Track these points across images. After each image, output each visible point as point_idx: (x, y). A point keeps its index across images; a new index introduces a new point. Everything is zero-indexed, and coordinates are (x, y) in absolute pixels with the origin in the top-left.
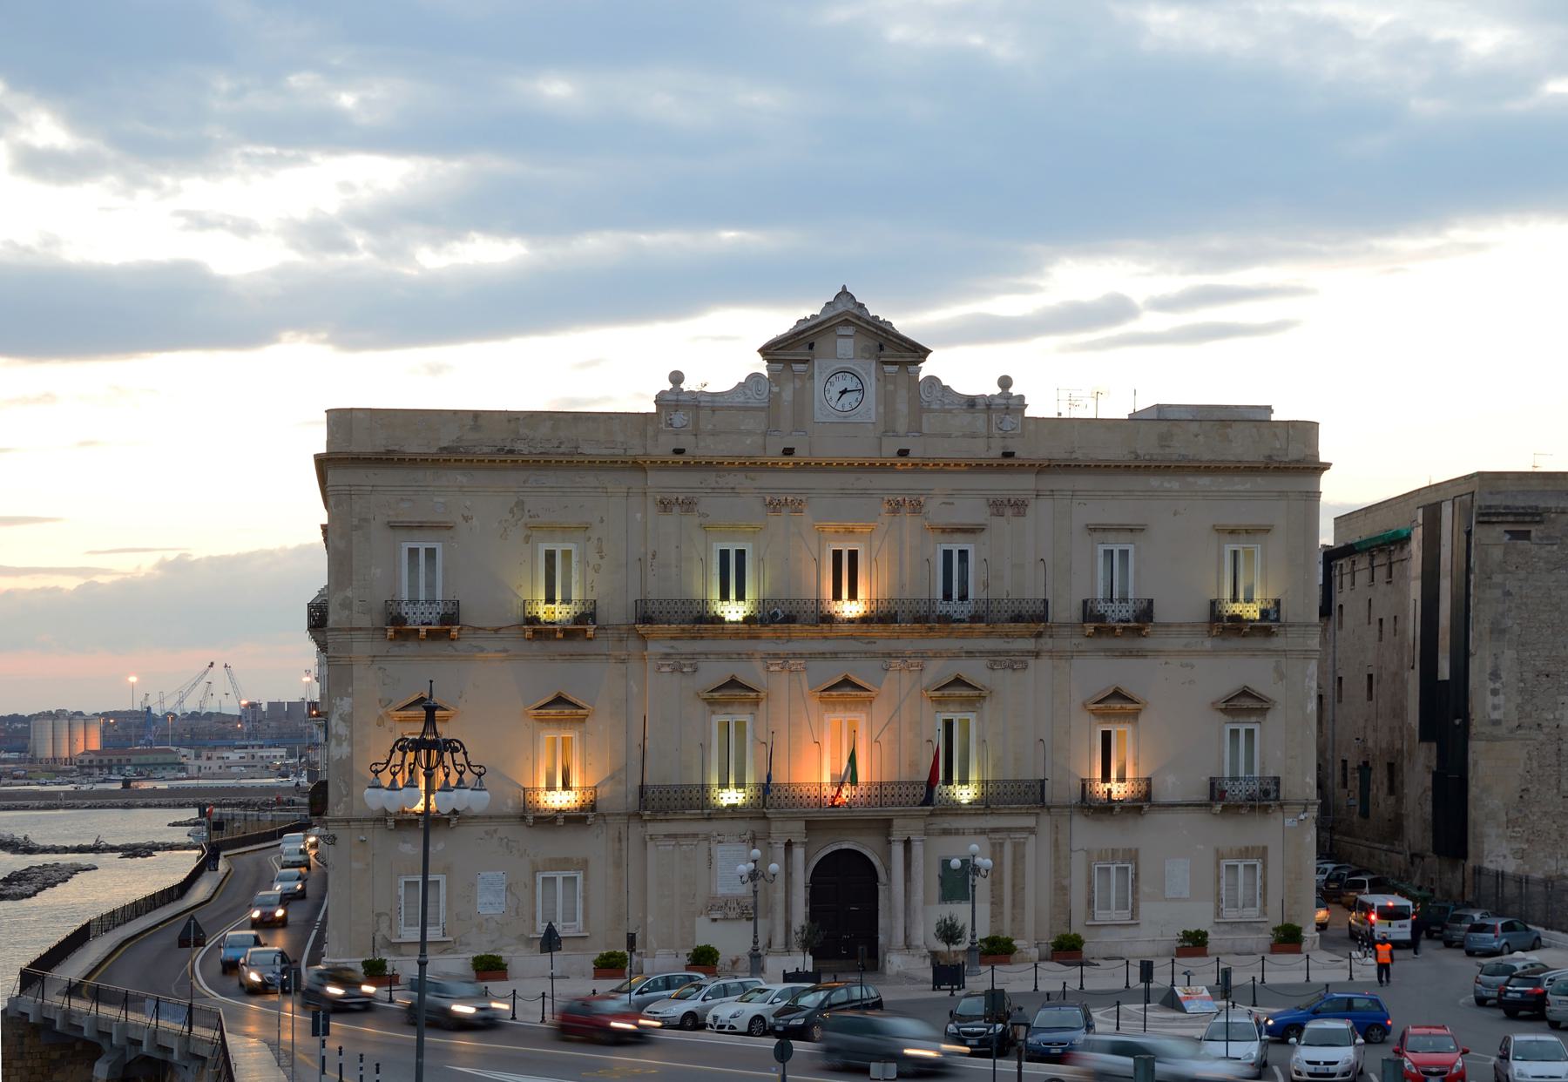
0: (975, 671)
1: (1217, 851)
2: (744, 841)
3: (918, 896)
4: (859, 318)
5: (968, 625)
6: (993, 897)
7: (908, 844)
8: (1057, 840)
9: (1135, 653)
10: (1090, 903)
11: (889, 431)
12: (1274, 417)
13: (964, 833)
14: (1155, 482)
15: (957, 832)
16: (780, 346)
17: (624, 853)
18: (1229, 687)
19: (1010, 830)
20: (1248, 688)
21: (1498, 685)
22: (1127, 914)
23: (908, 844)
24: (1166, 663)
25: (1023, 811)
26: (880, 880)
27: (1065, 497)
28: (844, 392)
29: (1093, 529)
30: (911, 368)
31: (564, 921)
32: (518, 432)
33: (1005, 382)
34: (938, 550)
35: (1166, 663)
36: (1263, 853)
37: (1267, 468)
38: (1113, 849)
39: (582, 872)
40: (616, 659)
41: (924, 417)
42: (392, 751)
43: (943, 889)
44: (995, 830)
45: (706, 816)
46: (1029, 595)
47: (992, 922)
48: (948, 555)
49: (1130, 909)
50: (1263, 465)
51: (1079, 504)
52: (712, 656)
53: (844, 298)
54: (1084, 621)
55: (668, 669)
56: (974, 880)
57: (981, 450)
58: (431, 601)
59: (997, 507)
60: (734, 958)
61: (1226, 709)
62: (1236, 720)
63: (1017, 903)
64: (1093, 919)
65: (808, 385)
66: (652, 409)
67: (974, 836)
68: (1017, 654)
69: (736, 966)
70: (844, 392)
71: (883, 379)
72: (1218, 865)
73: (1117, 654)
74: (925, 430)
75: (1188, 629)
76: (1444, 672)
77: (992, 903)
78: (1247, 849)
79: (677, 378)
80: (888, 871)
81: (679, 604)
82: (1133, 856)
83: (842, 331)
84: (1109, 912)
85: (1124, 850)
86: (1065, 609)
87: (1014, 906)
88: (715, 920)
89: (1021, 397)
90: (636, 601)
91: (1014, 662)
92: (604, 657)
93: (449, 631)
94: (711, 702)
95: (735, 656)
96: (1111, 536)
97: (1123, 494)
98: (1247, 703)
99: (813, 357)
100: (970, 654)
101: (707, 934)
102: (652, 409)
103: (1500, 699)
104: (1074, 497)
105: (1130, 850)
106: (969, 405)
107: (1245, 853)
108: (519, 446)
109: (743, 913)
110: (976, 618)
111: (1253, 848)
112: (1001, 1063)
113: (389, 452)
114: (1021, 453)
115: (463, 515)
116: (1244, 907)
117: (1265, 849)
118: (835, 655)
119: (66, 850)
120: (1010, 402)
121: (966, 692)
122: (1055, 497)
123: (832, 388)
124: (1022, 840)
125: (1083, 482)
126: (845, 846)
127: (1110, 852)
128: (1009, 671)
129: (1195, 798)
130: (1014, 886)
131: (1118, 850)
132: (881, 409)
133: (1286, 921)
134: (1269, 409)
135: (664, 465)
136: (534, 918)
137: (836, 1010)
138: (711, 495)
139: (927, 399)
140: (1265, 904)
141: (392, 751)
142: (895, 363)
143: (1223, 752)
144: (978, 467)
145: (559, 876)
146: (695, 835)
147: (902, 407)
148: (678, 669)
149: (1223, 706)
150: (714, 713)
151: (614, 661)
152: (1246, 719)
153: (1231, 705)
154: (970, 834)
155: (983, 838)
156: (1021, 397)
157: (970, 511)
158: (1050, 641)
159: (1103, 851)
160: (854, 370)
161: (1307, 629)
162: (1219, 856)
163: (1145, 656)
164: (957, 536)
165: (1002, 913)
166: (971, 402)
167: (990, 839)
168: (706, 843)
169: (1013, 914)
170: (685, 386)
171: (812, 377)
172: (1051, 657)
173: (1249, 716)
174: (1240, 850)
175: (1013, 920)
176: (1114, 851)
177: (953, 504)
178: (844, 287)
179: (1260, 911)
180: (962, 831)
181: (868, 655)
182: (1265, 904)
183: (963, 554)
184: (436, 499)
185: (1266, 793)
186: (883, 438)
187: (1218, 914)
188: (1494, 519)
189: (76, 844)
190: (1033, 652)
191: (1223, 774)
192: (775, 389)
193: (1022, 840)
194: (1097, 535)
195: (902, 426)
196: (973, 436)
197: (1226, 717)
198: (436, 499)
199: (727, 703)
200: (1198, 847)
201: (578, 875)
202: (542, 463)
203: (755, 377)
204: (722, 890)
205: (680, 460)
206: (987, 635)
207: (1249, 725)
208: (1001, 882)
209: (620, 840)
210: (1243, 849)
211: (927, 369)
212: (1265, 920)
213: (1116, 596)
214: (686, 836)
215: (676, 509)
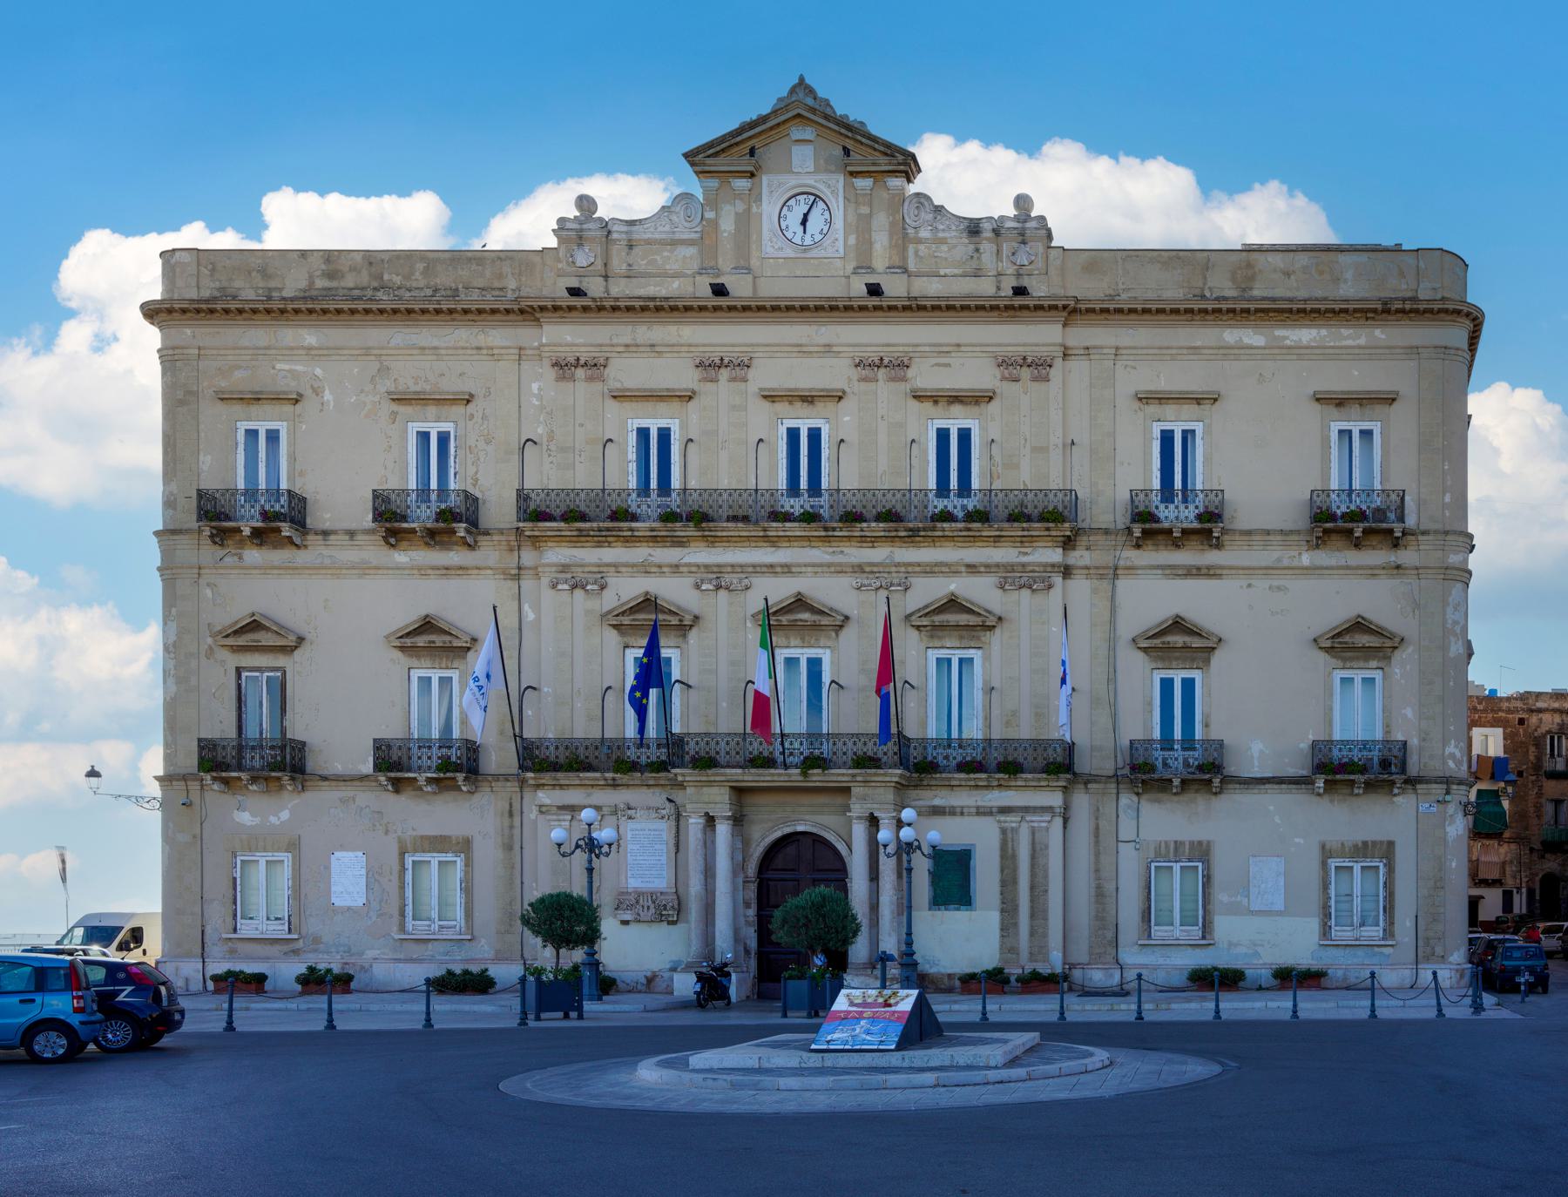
0: (980, 591)
1: (1323, 847)
2: (663, 818)
4: (813, 110)
5: (961, 525)
6: (1003, 903)
8: (1097, 828)
9: (1204, 571)
11: (864, 267)
13: (962, 814)
14: (1232, 335)
15: (952, 812)
16: (711, 151)
17: (517, 832)
18: (1338, 614)
19: (1026, 810)
20: (1363, 618)
22: (1196, 931)
24: (1249, 585)
25: (1043, 784)
27: (1105, 357)
28: (804, 222)
29: (1145, 399)
32: (382, 278)
34: (930, 428)
35: (1249, 585)
36: (1387, 851)
38: (1176, 842)
39: (462, 855)
40: (504, 574)
41: (911, 249)
43: (935, 890)
44: (1005, 810)
45: (610, 782)
47: (1003, 936)
48: (943, 435)
49: (1200, 925)
50: (1379, 307)
51: (1126, 366)
52: (623, 569)
55: (566, 587)
56: (909, 862)
60: (649, 974)
61: (1332, 648)
62: (1348, 665)
63: (1038, 912)
64: (1149, 936)
65: (754, 209)
66: (552, 242)
67: (976, 818)
68: (1037, 569)
69: (652, 984)
70: (804, 222)
71: (852, 198)
72: (1324, 864)
73: (1180, 573)
74: (912, 267)
75: (1279, 538)
77: (1002, 911)
78: (1365, 843)
81: (572, 495)
82: (1202, 852)
83: (797, 132)
84: (1172, 928)
85: (1191, 843)
87: (1033, 916)
88: (625, 923)
92: (489, 572)
95: (653, 569)
96: (1170, 410)
97: (1185, 351)
98: (1363, 640)
99: (758, 168)
100: (972, 569)
104: (1119, 357)
105: (1200, 843)
106: (970, 232)
107: (1363, 850)
109: (662, 915)
110: (972, 516)
111: (1374, 843)
112: (982, 475)
114: (1039, 289)
115: (312, 386)
116: (1363, 924)
117: (1391, 844)
118: (787, 569)
121: (963, 619)
122: (1092, 357)
123: (788, 214)
124: (1044, 824)
126: (800, 828)
127: (1172, 846)
128: (1026, 593)
129: (1291, 771)
130: (1032, 888)
131: (1182, 843)
132: (852, 240)
138: (624, 355)
139: (914, 224)
143: (1331, 709)
145: (435, 859)
149: (1328, 644)
151: (502, 577)
152: (1362, 664)
153: (1340, 643)
154: (969, 814)
157: (974, 374)
158: (1086, 554)
159: (1163, 845)
160: (814, 187)
161: (1448, 538)
162: (1326, 853)
163: (1219, 576)
164: (957, 409)
165: (1016, 925)
167: (999, 822)
168: (615, 817)
169: (1032, 927)
172: (1088, 577)
173: (1366, 659)
174: (1356, 846)
175: (1032, 934)
176: (1178, 845)
177: (949, 365)
178: (802, 79)
179: (1385, 930)
180: (958, 810)
181: (832, 569)
182: (1390, 922)
183: (965, 435)
184: (278, 366)
185: (1385, 764)
186: (853, 277)
187: (1324, 935)
190: (1059, 567)
191: (1331, 735)
192: (710, 215)
193: (1044, 824)
194: (1153, 409)
197: (1334, 660)
198: (278, 366)
200: (1297, 840)
201: (458, 859)
204: (633, 883)
207: (1367, 671)
208: (1015, 881)
209: (511, 814)
210: (1360, 844)
212: (1390, 943)
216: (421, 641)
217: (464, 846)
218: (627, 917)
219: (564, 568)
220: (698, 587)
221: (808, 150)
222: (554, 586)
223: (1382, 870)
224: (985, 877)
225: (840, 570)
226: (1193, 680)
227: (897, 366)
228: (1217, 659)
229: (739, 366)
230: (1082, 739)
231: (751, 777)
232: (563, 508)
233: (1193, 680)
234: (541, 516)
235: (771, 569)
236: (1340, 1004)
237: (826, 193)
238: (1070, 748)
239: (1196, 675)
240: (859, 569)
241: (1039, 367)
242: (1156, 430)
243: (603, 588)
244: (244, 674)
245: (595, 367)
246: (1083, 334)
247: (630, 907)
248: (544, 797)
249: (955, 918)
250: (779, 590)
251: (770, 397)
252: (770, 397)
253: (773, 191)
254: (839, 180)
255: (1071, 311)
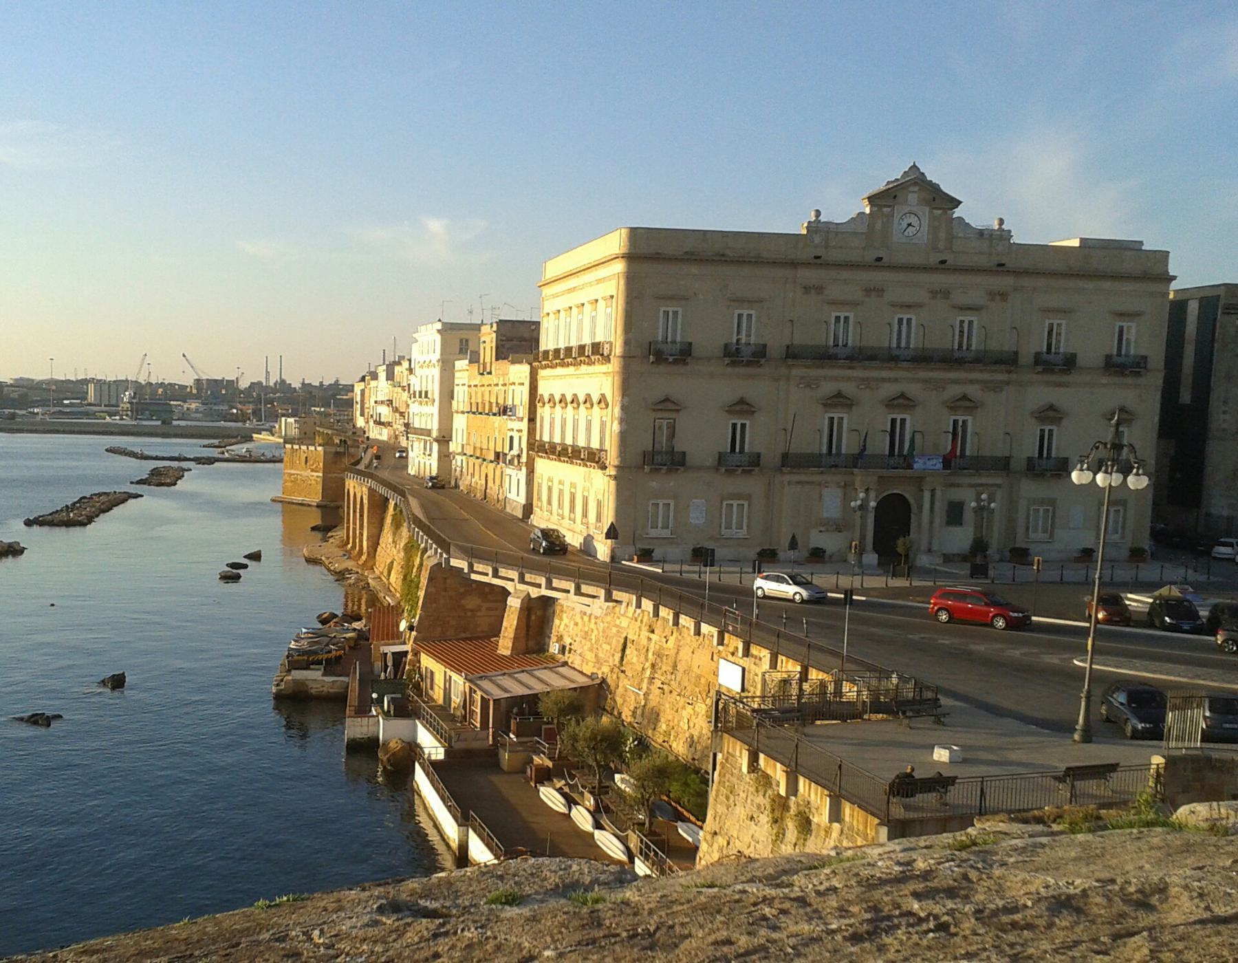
3: (937, 522)
7: (933, 491)
10: (1027, 529)
11: (935, 249)
12: (1143, 248)
14: (1081, 284)
15: (959, 486)
21: (1227, 409)
22: (1047, 535)
23: (933, 491)
26: (912, 511)
30: (949, 212)
31: (737, 529)
33: (1001, 221)
37: (1144, 278)
42: (1092, 449)
46: (1006, 348)
53: (914, 169)
54: (725, 356)
57: (983, 261)
58: (674, 342)
59: (868, 291)
76: (1186, 397)
79: (818, 213)
80: (920, 507)
82: (1052, 502)
83: (911, 189)
86: (1026, 358)
88: (821, 531)
89: (1009, 231)
90: (650, 343)
91: (996, 388)
93: (758, 362)
94: (951, 408)
98: (1051, 414)
100: (972, 382)
101: (818, 539)
102: (805, 232)
103: (1227, 417)
108: (728, 252)
113: (658, 254)
118: (896, 380)
119: (163, 459)
120: (1003, 233)
121: (968, 404)
125: (1041, 282)
126: (895, 492)
133: (1135, 545)
134: (1141, 243)
135: (807, 264)
136: (720, 527)
137: (512, 551)
140: (1123, 533)
141: (1092, 449)
142: (940, 209)
144: (926, 269)
145: (735, 503)
146: (812, 483)
147: (942, 235)
148: (808, 385)
150: (826, 412)
155: (973, 489)
156: (1009, 231)
166: (981, 233)
170: (823, 218)
171: (893, 216)
188: (1232, 312)
189: (169, 455)
195: (941, 245)
196: (981, 253)
199: (835, 406)
202: (740, 261)
203: (861, 214)
204: (825, 515)
205: (817, 261)
206: (981, 371)
211: (958, 213)
213: (669, 340)
214: (808, 483)
215: (813, 291)
216: (738, 408)
217: (748, 498)
218: (823, 529)
219: (802, 378)
220: (858, 387)
221: (916, 196)
222: (798, 386)
223: (1122, 511)
224: (969, 516)
225: (918, 381)
226: (745, 424)
227: (946, 294)
228: (1064, 423)
229: (880, 291)
230: (763, 451)
231: (885, 472)
232: (845, 356)
233: (745, 424)
234: (795, 357)
235: (889, 380)
236: (678, 575)
237: (920, 214)
238: (759, 455)
239: (1054, 428)
240: (926, 381)
241: (1003, 296)
242: (1047, 322)
243: (818, 387)
244: (657, 421)
245: (820, 289)
246: (1025, 282)
247: (825, 525)
248: (787, 478)
249: (956, 530)
250: (958, 390)
251: (893, 305)
252: (893, 305)
253: (899, 210)
254: (927, 209)
255: (1018, 273)
